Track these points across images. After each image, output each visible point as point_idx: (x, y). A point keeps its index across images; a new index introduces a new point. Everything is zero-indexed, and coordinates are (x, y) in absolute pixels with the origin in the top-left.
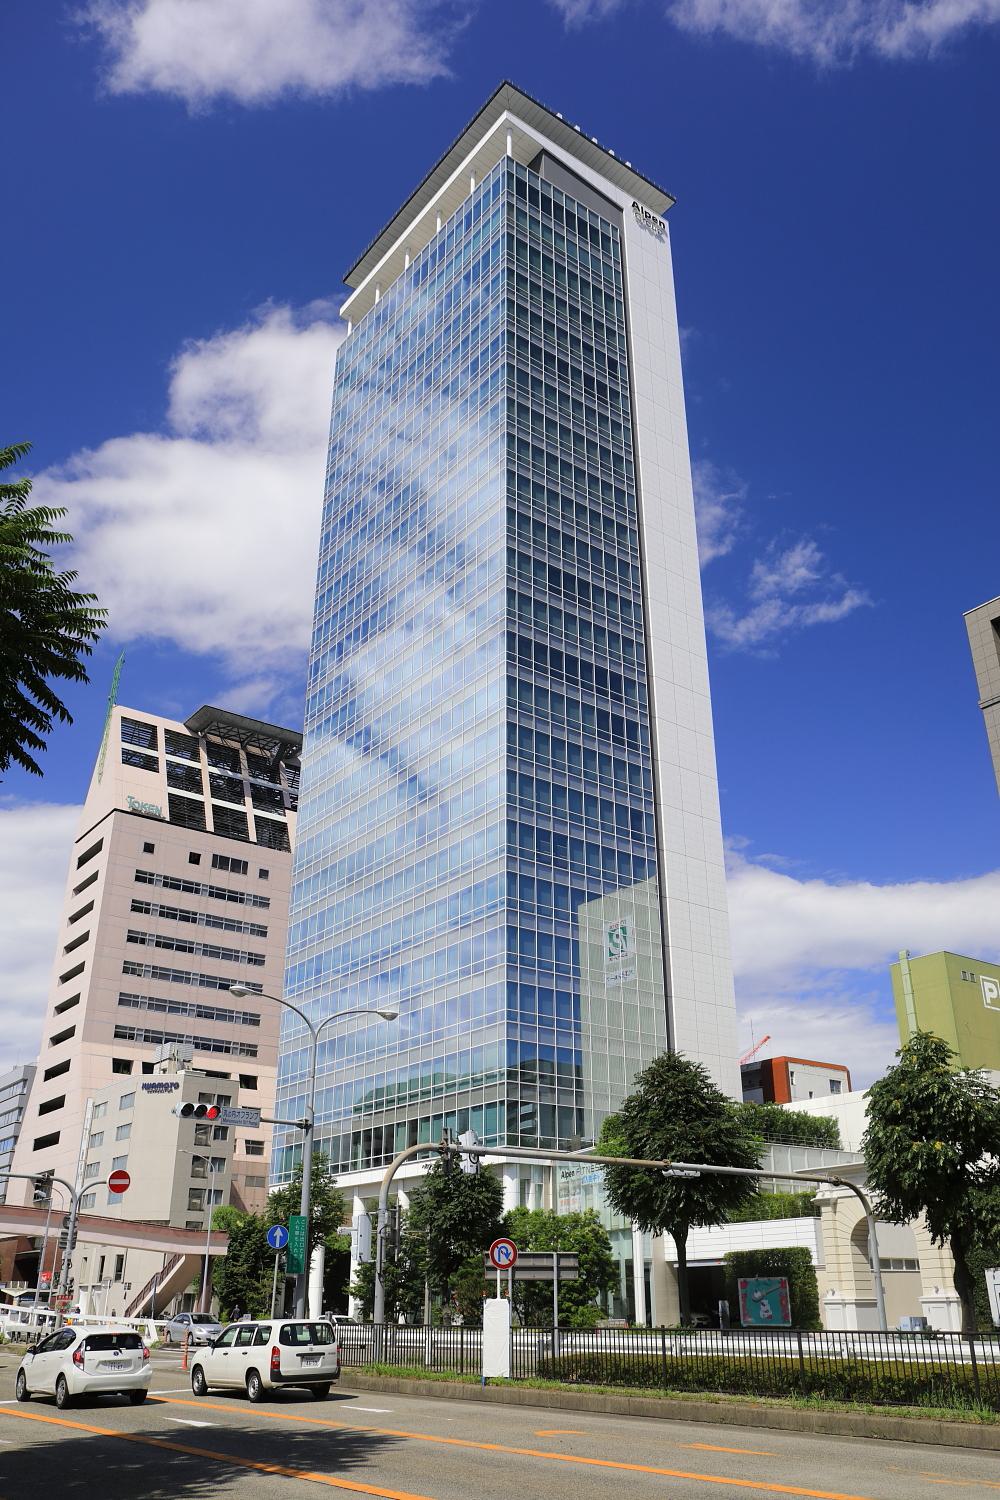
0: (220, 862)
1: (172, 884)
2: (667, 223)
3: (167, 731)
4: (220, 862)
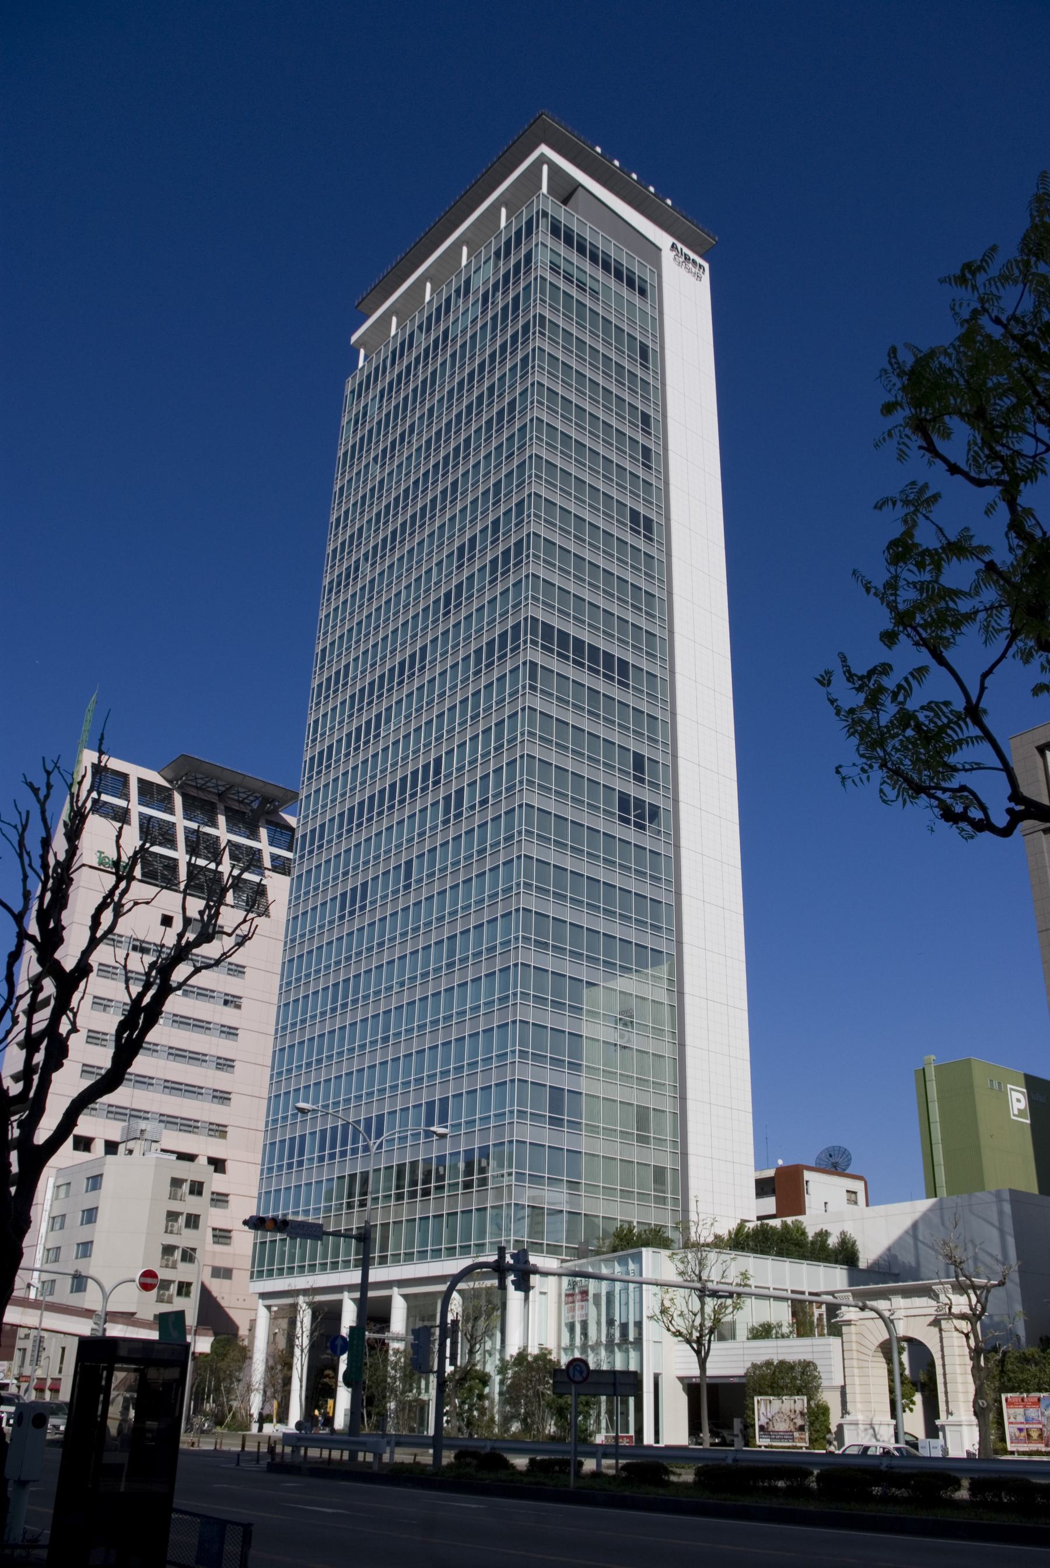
2: (706, 265)
3: (140, 781)
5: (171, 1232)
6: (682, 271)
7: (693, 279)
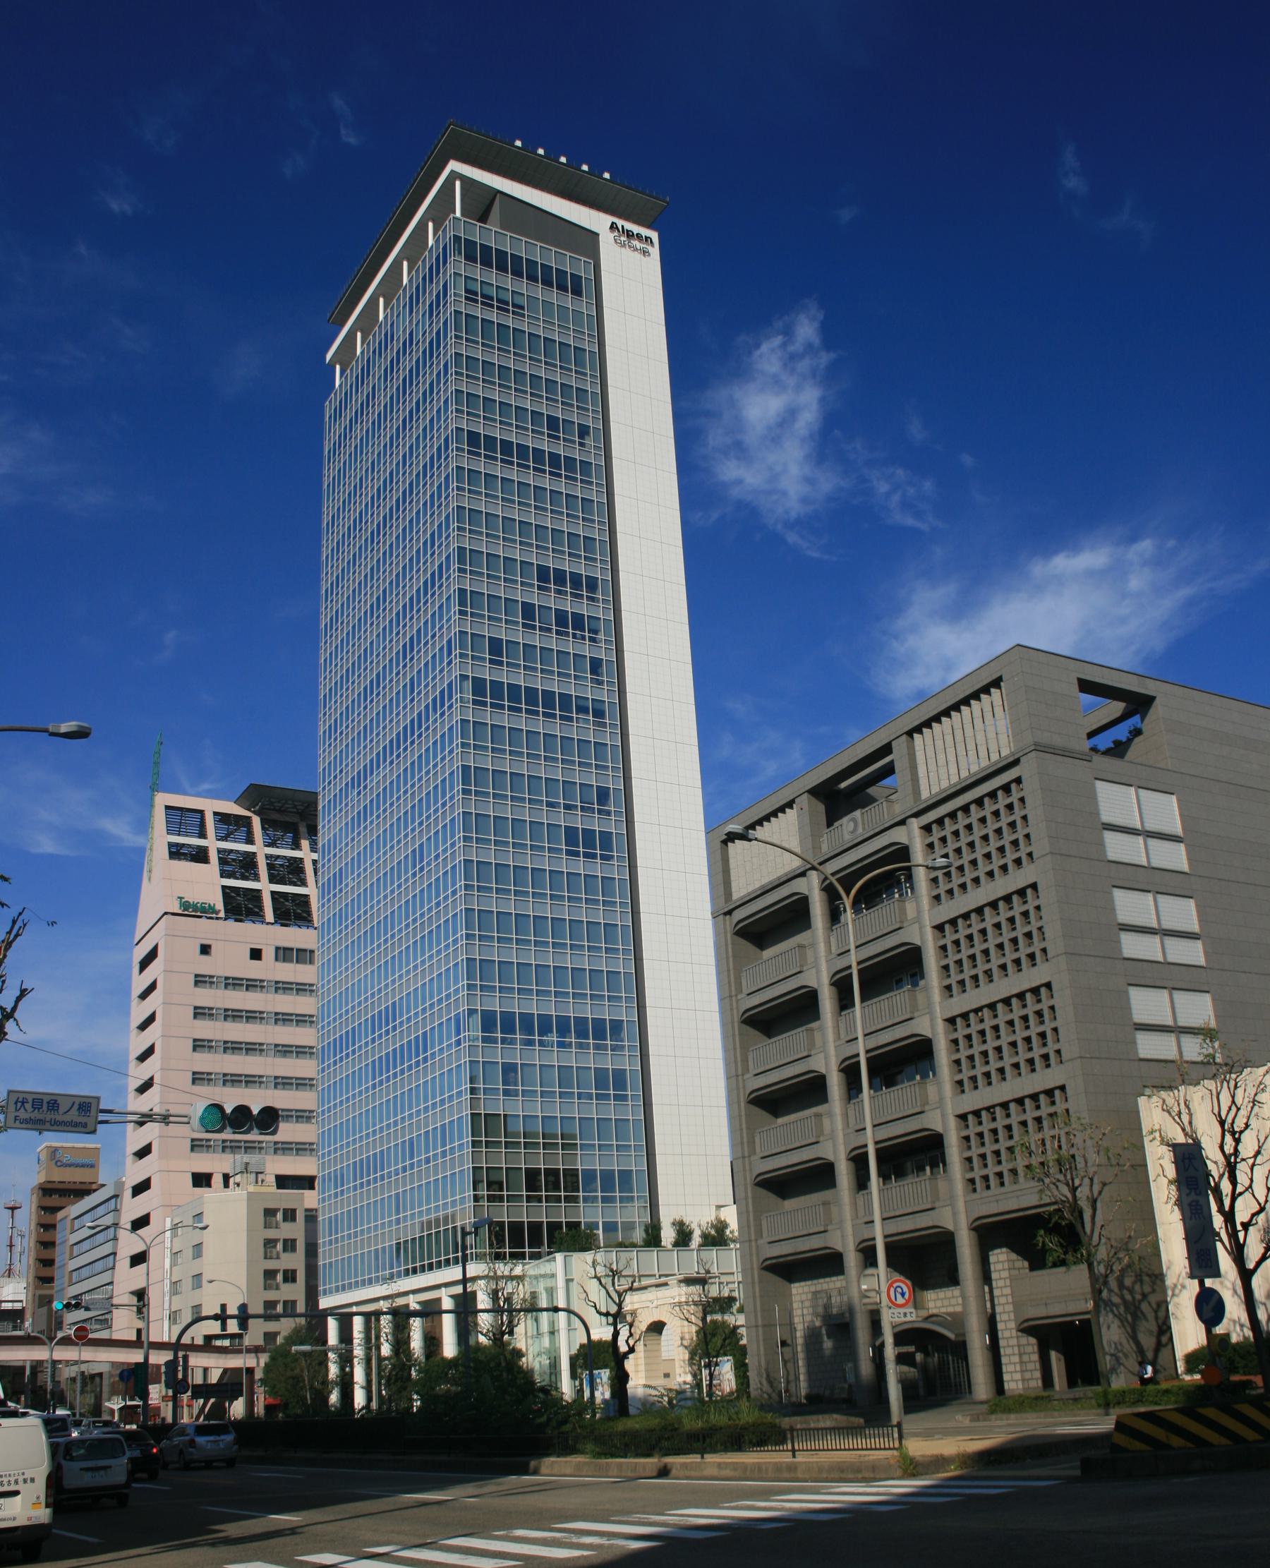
0: (284, 954)
1: (232, 983)
2: (654, 235)
4: (284, 954)
5: (271, 1258)
6: (626, 252)
7: (637, 255)
